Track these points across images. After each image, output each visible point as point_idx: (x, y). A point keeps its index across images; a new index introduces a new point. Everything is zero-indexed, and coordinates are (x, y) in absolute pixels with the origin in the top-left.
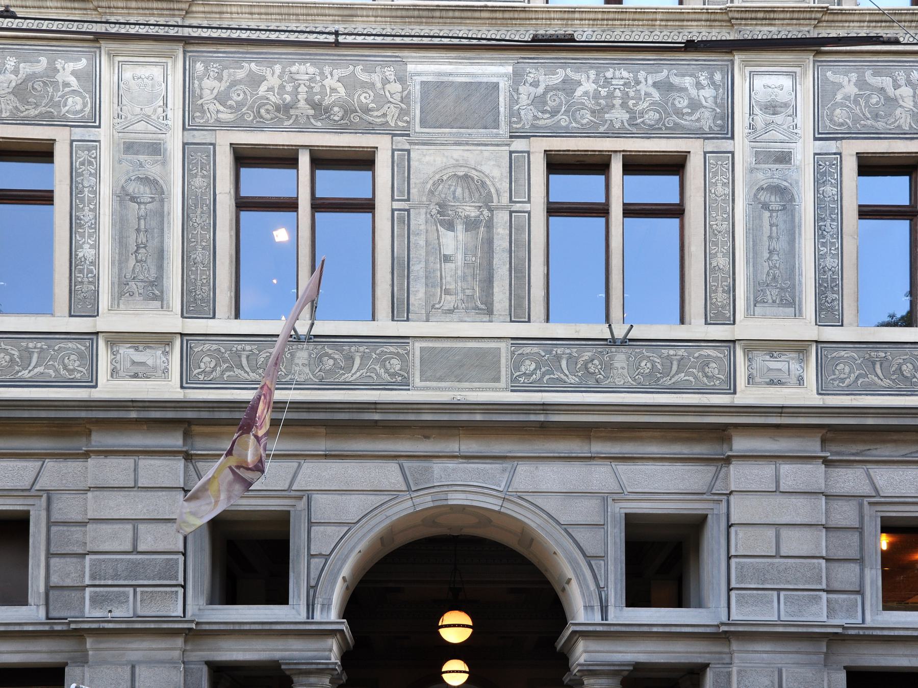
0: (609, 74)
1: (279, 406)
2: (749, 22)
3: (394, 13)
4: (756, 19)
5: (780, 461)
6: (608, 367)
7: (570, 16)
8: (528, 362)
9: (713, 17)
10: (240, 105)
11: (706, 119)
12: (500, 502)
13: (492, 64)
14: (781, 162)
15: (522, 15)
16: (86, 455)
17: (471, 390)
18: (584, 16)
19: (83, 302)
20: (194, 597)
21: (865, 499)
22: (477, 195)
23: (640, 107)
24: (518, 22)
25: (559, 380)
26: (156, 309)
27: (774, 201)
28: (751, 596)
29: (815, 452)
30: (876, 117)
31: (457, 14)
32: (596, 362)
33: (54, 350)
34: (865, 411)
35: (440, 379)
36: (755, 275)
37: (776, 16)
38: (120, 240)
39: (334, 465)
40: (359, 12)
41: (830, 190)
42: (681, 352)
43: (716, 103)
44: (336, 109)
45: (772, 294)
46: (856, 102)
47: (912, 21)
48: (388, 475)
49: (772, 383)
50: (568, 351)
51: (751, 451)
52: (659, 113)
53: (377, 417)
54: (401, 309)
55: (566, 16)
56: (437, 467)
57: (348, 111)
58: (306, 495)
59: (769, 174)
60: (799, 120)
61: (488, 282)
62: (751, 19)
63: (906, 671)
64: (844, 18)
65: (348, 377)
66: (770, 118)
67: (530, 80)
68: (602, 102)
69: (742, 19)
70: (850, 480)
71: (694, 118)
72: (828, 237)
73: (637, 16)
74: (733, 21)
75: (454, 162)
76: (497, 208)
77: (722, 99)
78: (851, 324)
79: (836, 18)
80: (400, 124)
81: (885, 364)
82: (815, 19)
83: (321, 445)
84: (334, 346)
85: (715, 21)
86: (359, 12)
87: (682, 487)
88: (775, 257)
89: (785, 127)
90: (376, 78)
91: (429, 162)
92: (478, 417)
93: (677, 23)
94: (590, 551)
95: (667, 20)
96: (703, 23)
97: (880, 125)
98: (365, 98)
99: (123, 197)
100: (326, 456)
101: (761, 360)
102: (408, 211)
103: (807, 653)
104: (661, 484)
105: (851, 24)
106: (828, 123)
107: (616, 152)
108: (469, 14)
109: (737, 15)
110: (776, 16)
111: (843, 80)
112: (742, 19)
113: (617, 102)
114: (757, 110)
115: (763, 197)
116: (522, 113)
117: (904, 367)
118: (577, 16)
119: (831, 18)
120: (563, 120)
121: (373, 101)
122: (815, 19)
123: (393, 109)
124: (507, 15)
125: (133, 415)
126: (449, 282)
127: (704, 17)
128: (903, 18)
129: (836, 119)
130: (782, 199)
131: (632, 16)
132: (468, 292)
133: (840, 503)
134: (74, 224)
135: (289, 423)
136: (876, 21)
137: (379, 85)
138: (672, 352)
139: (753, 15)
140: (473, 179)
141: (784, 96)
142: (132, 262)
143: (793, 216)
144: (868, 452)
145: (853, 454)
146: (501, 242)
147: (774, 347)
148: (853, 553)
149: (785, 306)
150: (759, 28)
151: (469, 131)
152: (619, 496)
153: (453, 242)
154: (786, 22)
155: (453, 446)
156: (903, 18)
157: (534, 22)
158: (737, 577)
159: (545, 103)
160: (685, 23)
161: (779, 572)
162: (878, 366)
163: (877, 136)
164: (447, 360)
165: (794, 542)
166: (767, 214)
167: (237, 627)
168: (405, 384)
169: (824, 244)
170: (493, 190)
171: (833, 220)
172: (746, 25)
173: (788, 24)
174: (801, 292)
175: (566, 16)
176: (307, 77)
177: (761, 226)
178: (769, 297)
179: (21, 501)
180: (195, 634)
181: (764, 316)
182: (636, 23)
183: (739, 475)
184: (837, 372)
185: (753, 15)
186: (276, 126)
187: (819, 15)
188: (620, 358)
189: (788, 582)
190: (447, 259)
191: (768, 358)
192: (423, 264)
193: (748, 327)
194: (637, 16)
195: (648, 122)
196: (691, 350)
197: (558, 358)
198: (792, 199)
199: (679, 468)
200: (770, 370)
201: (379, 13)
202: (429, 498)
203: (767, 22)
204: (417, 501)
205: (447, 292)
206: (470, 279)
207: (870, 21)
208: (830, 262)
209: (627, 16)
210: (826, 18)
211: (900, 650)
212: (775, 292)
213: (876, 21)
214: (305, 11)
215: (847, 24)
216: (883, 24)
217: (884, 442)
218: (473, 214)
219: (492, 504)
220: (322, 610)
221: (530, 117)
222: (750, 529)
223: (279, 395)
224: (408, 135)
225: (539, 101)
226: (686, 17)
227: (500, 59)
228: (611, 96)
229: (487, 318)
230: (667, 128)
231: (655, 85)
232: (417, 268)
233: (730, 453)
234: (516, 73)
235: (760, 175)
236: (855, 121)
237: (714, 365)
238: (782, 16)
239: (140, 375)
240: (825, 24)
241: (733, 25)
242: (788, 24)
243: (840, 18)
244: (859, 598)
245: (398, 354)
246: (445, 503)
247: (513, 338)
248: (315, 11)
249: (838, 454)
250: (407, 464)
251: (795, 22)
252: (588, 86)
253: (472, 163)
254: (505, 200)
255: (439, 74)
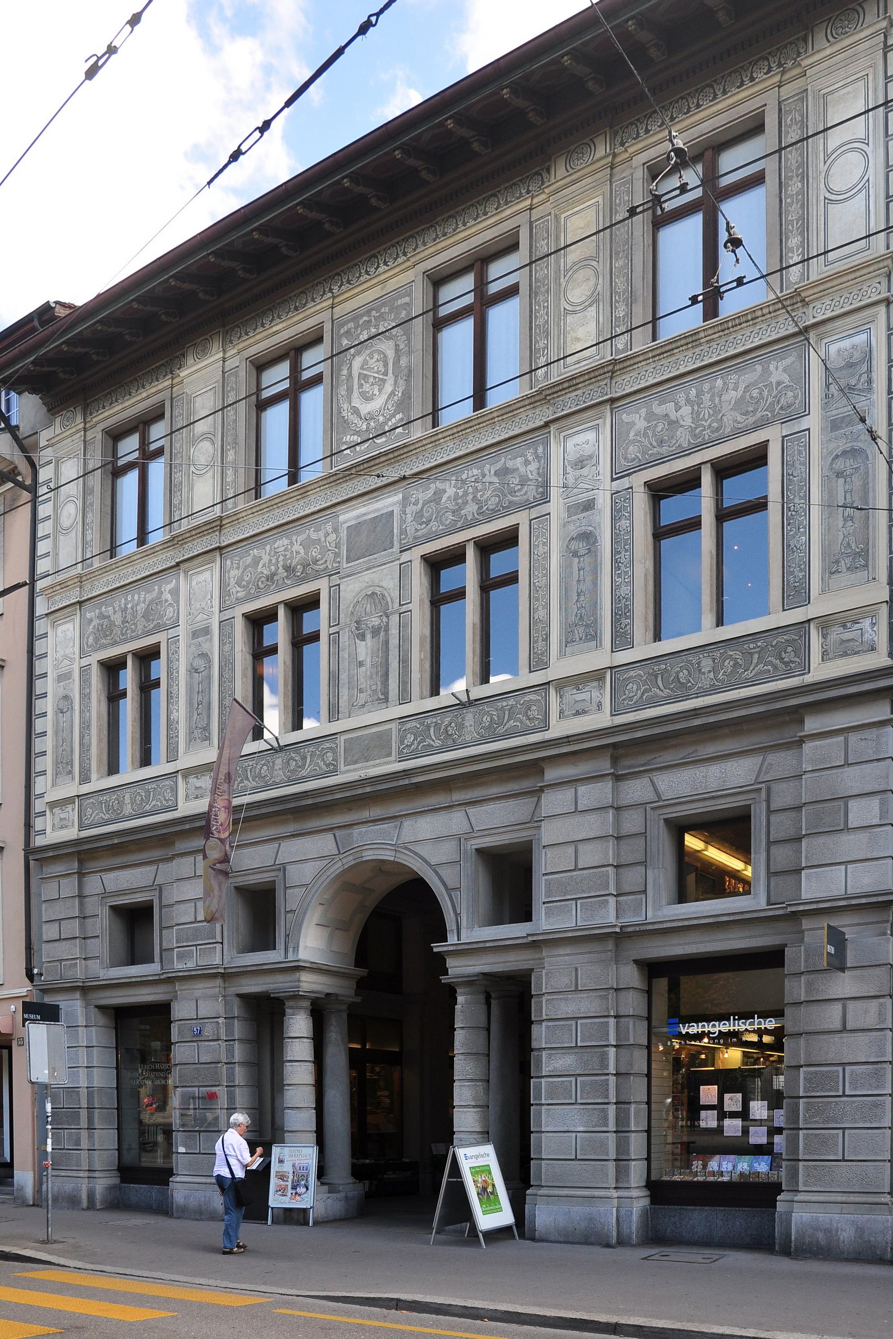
0: (464, 476)
1: (238, 809)
2: (560, 393)
3: (329, 481)
4: (564, 389)
5: (579, 784)
6: (461, 727)
7: (436, 438)
8: (409, 735)
9: (533, 400)
10: (248, 582)
11: (531, 492)
12: (393, 853)
13: (390, 497)
14: (587, 510)
15: (406, 450)
16: (173, 858)
17: (374, 766)
18: (445, 434)
19: (796, 593)
20: (229, 950)
21: (648, 806)
22: (379, 606)
23: (485, 497)
24: (405, 456)
25: (429, 745)
26: (206, 747)
27: (581, 547)
28: (556, 907)
29: (606, 769)
30: (661, 443)
31: (366, 466)
32: (453, 725)
33: (772, 646)
34: (632, 726)
35: (356, 762)
36: (566, 618)
37: (578, 381)
38: (190, 703)
39: (297, 842)
40: (309, 488)
41: (624, 523)
42: (512, 702)
43: (539, 474)
44: (299, 567)
45: (197, 733)
46: (645, 435)
47: (687, 344)
48: (325, 844)
49: (578, 713)
50: (434, 720)
51: (558, 779)
52: (499, 497)
53: (310, 802)
54: (334, 714)
55: (433, 439)
56: (356, 831)
57: (305, 566)
58: (283, 868)
59: (580, 523)
60: (601, 468)
61: (386, 675)
62: (560, 391)
63: (717, 955)
64: (632, 362)
65: (304, 773)
66: (578, 473)
67: (413, 500)
68: (460, 501)
69: (553, 393)
70: (637, 790)
71: (522, 493)
72: (623, 568)
73: (480, 420)
74: (548, 398)
75: (366, 584)
76: (392, 613)
77: (544, 468)
78: (639, 645)
79: (625, 364)
80: (335, 565)
81: (666, 675)
82: (608, 372)
83: (291, 828)
84: (297, 751)
85: (535, 402)
86: (309, 488)
87: (513, 819)
88: (582, 598)
89: (590, 477)
90: (321, 534)
91: (351, 589)
92: (368, 790)
93: (510, 415)
94: (451, 885)
95: (502, 415)
96: (528, 407)
97: (664, 450)
98: (315, 553)
99: (193, 670)
100: (293, 836)
101: (571, 695)
102: (338, 633)
103: (597, 952)
104: (495, 819)
105: (640, 365)
106: (623, 462)
107: (468, 541)
108: (372, 463)
109: (548, 392)
110: (578, 381)
111: (635, 417)
112: (553, 393)
113: (470, 497)
114: (569, 470)
115: (574, 546)
116: (408, 529)
117: (681, 674)
118: (440, 436)
119: (621, 366)
120: (434, 526)
121: (319, 554)
122: (608, 372)
123: (331, 555)
124: (396, 454)
125: (187, 826)
126: (363, 685)
127: (527, 402)
128: (679, 344)
129: (629, 456)
130: (588, 544)
131: (476, 422)
132: (374, 688)
133: (630, 812)
134: (169, 694)
135: (247, 820)
136: (658, 355)
137: (323, 539)
138: (505, 704)
139: (561, 387)
140: (376, 594)
141: (588, 450)
142: (195, 716)
143: (596, 556)
144: (654, 761)
145: (642, 765)
146: (394, 642)
147: (579, 681)
148: (640, 857)
149: (590, 640)
150: (569, 395)
151: (375, 556)
152: (472, 833)
153: (365, 649)
154: (587, 383)
155: (365, 814)
156: (679, 344)
157: (414, 452)
158: (546, 892)
159: (422, 516)
160: (515, 412)
161: (577, 883)
162: (660, 678)
163: (662, 460)
164: (373, 744)
165: (590, 855)
166: (576, 560)
167: (481, 945)
168: (334, 771)
169: (619, 576)
170: (389, 600)
171: (626, 551)
172: (558, 397)
173: (589, 384)
174: (601, 624)
175: (433, 439)
176: (283, 549)
177: (571, 573)
178: (577, 636)
179: (144, 894)
180: (227, 976)
181: (573, 654)
182: (481, 425)
183: (555, 801)
184: (627, 692)
185: (561, 387)
186: (267, 591)
187: (610, 368)
188: (469, 717)
189: (584, 891)
190: (361, 664)
191: (575, 691)
192: (347, 673)
193: (561, 667)
194: (480, 420)
195: (491, 507)
196: (517, 698)
197: (428, 727)
198: (596, 541)
199: (512, 803)
200: (576, 702)
201: (321, 483)
202: (351, 858)
203: (573, 388)
204: (344, 861)
205: (361, 691)
206: (374, 676)
207: (653, 357)
208: (624, 590)
209: (473, 423)
210: (617, 367)
211: (675, 940)
212: (581, 629)
213: (658, 355)
214: (208, 527)
215: (636, 366)
216: (665, 355)
217: (666, 748)
218: (377, 623)
219: (388, 855)
220: (294, 951)
221: (413, 531)
222: (556, 848)
223: (236, 802)
224: (339, 573)
225: (419, 515)
226: (514, 407)
227: (395, 490)
228: (466, 494)
229: (384, 705)
230: (504, 508)
231: (496, 474)
232: (344, 677)
233: (802, 734)
234: (404, 498)
235: (571, 527)
236: (644, 453)
237: (535, 708)
238: (582, 379)
239: (849, 652)
240: (619, 373)
241: (549, 401)
242: (589, 384)
243: (628, 363)
244: (644, 896)
245: (331, 748)
246: (360, 860)
247: (399, 718)
248: (285, 497)
249: (630, 767)
250: (338, 833)
251: (593, 380)
252: (450, 491)
253: (376, 582)
254: (396, 605)
255: (358, 517)
